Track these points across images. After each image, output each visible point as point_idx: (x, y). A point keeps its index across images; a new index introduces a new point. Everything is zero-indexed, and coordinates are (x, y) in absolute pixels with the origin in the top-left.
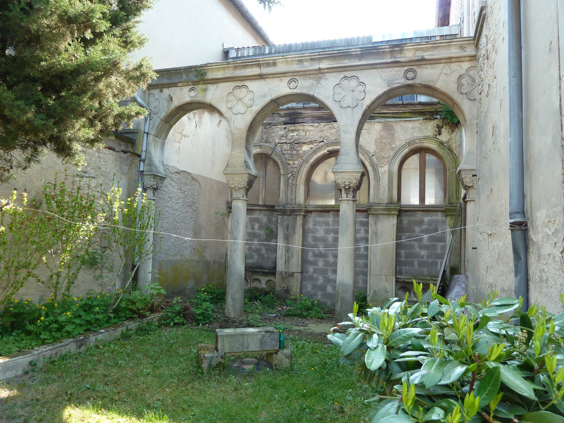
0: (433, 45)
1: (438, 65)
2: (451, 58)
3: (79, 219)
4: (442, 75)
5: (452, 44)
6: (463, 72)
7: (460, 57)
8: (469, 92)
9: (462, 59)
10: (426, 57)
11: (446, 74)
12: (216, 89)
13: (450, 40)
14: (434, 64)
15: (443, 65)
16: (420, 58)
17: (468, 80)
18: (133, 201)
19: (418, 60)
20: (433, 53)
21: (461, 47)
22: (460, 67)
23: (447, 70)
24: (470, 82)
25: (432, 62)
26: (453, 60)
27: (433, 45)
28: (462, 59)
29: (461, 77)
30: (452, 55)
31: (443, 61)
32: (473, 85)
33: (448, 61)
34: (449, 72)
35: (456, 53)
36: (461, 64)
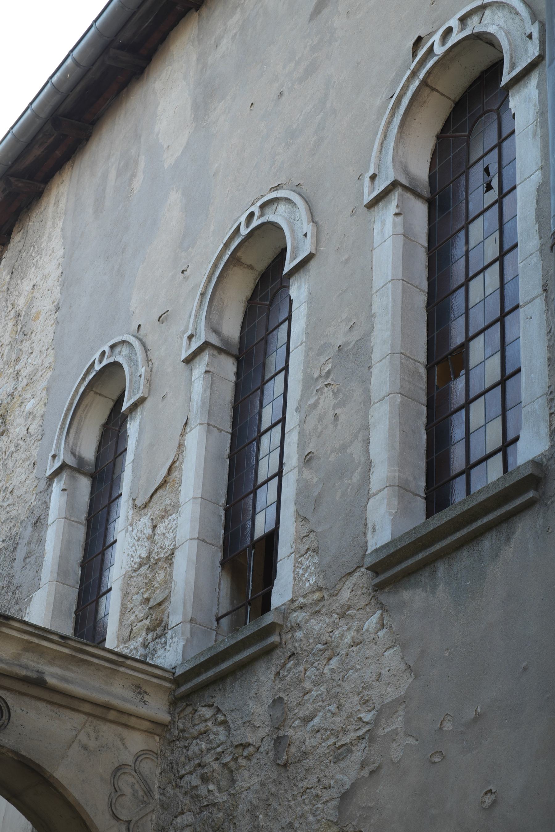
0: (74, 653)
1: (68, 713)
2: (107, 707)
3: (9, 528)
4: (75, 746)
5: (122, 669)
6: (127, 758)
7: (130, 715)
8: (135, 819)
9: (133, 721)
10: (51, 681)
11: (85, 747)
12: (71, 178)
13: (121, 660)
14: (61, 706)
15: (81, 718)
16: (34, 675)
17: (137, 786)
18: (16, 384)
19: (25, 680)
20: (68, 674)
21: (139, 687)
22: (122, 740)
23: (88, 735)
24: (141, 793)
25: (57, 699)
26: (112, 715)
27: (74, 653)
28: (133, 721)
29: (118, 770)
30: (115, 702)
31: (87, 708)
32: (146, 804)
33: (99, 711)
34: (92, 744)
35: (125, 700)
36: (125, 733)
